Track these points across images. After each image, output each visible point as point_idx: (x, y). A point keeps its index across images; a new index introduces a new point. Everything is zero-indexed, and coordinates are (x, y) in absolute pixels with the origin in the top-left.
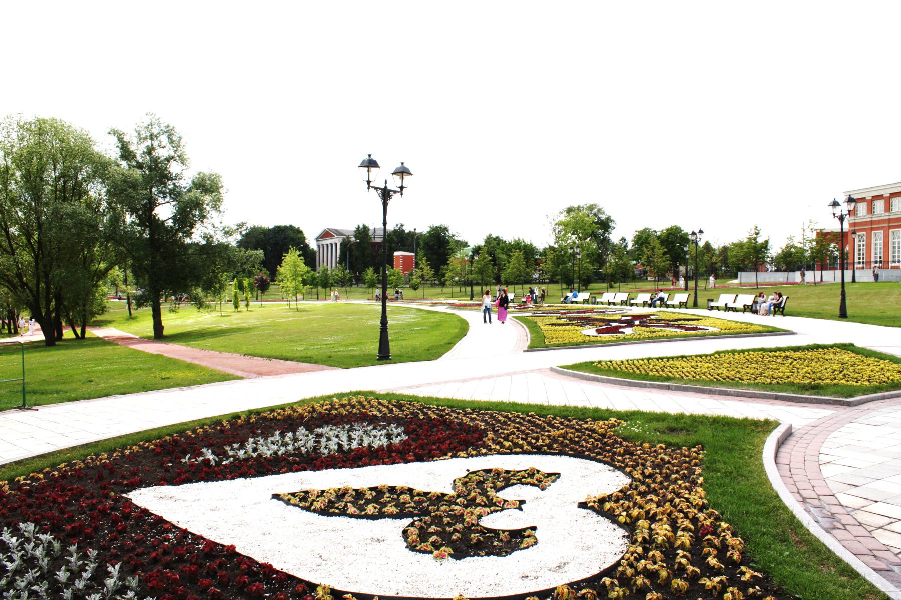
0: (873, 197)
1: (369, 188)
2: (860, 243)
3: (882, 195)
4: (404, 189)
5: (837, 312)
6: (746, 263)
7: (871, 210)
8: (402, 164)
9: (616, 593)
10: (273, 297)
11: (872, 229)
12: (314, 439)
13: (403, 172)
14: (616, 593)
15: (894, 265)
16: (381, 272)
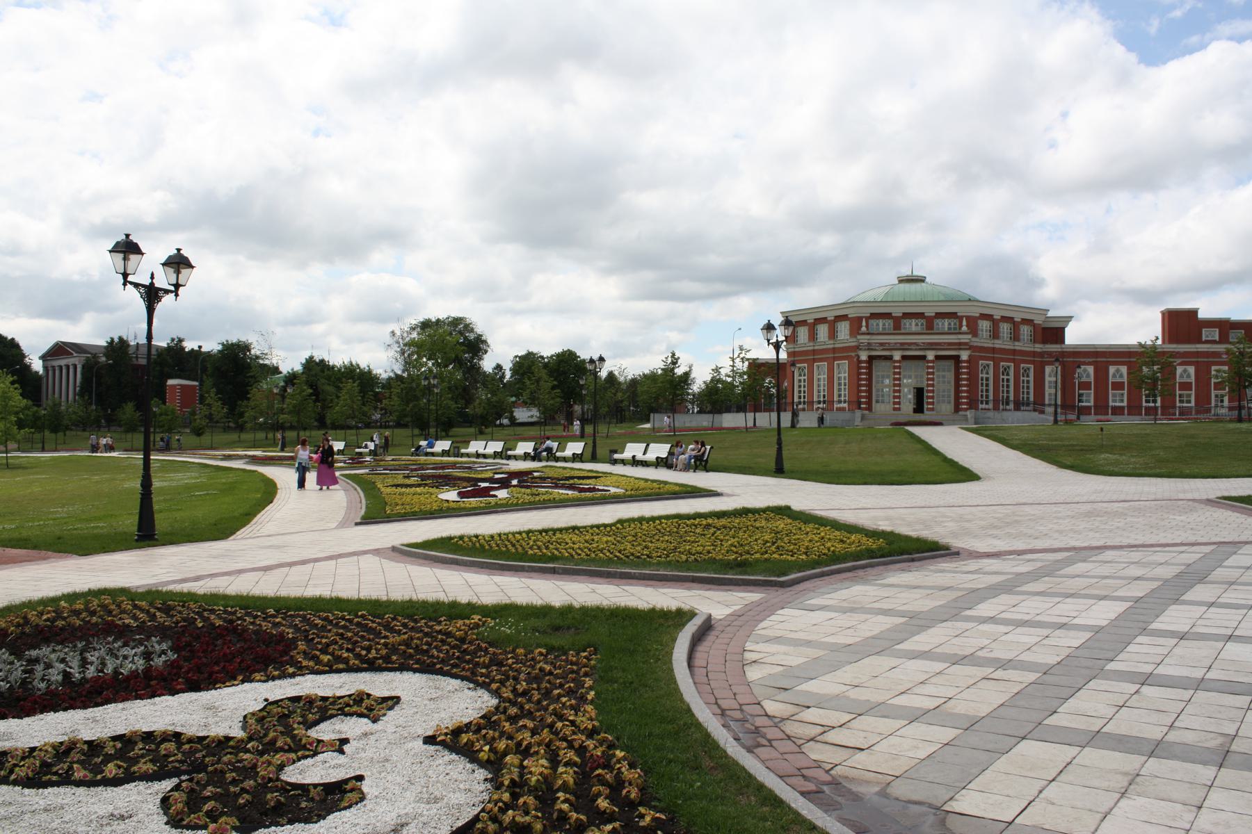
1: (125, 284)
4: (181, 288)
8: (127, 236)
13: (178, 262)
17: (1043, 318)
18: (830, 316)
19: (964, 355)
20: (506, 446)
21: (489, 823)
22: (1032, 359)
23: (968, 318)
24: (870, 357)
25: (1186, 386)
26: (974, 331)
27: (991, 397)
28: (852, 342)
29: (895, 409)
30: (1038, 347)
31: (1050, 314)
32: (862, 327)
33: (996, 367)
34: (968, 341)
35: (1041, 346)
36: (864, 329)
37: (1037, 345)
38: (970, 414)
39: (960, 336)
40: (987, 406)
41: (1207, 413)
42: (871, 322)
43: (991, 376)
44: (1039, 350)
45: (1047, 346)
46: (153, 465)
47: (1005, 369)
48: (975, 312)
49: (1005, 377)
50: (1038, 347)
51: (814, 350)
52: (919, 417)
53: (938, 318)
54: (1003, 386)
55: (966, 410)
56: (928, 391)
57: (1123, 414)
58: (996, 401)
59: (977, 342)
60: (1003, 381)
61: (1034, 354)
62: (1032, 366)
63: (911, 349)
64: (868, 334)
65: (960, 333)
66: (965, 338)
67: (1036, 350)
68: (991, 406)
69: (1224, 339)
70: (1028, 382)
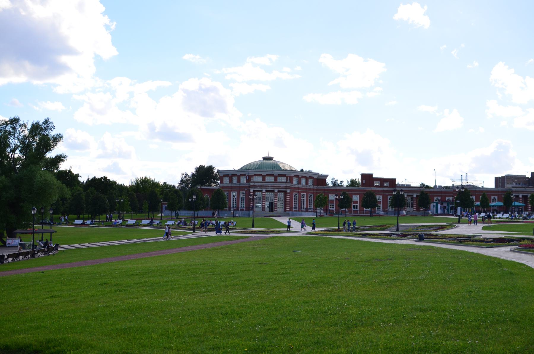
0: (240, 174)
2: (269, 198)
3: (262, 174)
5: (251, 225)
6: (98, 208)
7: (231, 181)
9: (481, 216)
10: (434, 237)
11: (240, 190)
12: (253, 352)
14: (481, 216)
15: (242, 208)
16: (164, 202)
17: (317, 176)
18: (230, 174)
19: (288, 191)
20: (160, 222)
21: (361, 323)
22: (313, 191)
23: (290, 177)
24: (254, 191)
25: (356, 202)
26: (291, 182)
27: (297, 207)
28: (247, 185)
29: (263, 210)
30: (315, 187)
31: (319, 174)
32: (251, 179)
33: (300, 195)
34: (289, 186)
35: (316, 187)
36: (252, 180)
37: (314, 186)
38: (290, 212)
39: (287, 184)
40: (296, 210)
41: (241, 209)
42: (254, 177)
43: (305, 198)
44: (315, 188)
45: (318, 187)
46: (35, 227)
47: (295, 195)
48: (292, 175)
49: (295, 198)
50: (315, 187)
51: (231, 186)
52: (271, 214)
53: (303, 178)
54: (309, 202)
55: (289, 211)
56: (275, 204)
57: (208, 210)
58: (299, 208)
59: (292, 186)
60: (309, 201)
61: (314, 189)
62: (245, 192)
63: (257, 188)
64: (253, 182)
65: (287, 183)
66: (288, 185)
67: (314, 188)
68: (297, 209)
69: (381, 185)
70: (311, 200)
